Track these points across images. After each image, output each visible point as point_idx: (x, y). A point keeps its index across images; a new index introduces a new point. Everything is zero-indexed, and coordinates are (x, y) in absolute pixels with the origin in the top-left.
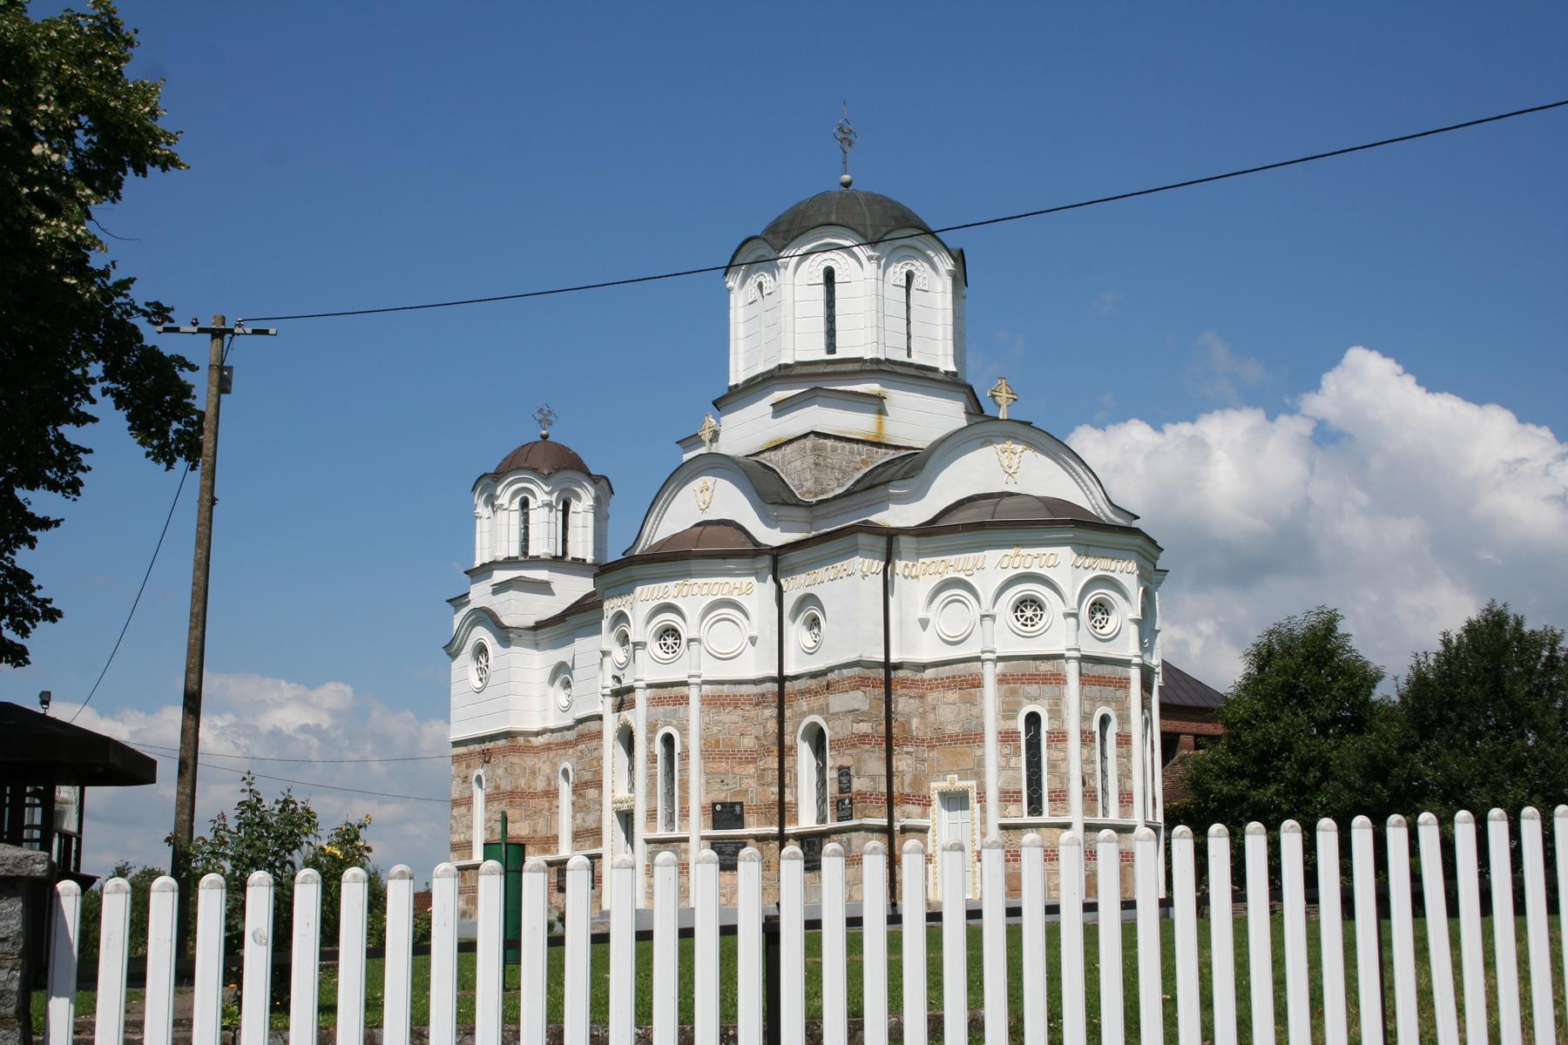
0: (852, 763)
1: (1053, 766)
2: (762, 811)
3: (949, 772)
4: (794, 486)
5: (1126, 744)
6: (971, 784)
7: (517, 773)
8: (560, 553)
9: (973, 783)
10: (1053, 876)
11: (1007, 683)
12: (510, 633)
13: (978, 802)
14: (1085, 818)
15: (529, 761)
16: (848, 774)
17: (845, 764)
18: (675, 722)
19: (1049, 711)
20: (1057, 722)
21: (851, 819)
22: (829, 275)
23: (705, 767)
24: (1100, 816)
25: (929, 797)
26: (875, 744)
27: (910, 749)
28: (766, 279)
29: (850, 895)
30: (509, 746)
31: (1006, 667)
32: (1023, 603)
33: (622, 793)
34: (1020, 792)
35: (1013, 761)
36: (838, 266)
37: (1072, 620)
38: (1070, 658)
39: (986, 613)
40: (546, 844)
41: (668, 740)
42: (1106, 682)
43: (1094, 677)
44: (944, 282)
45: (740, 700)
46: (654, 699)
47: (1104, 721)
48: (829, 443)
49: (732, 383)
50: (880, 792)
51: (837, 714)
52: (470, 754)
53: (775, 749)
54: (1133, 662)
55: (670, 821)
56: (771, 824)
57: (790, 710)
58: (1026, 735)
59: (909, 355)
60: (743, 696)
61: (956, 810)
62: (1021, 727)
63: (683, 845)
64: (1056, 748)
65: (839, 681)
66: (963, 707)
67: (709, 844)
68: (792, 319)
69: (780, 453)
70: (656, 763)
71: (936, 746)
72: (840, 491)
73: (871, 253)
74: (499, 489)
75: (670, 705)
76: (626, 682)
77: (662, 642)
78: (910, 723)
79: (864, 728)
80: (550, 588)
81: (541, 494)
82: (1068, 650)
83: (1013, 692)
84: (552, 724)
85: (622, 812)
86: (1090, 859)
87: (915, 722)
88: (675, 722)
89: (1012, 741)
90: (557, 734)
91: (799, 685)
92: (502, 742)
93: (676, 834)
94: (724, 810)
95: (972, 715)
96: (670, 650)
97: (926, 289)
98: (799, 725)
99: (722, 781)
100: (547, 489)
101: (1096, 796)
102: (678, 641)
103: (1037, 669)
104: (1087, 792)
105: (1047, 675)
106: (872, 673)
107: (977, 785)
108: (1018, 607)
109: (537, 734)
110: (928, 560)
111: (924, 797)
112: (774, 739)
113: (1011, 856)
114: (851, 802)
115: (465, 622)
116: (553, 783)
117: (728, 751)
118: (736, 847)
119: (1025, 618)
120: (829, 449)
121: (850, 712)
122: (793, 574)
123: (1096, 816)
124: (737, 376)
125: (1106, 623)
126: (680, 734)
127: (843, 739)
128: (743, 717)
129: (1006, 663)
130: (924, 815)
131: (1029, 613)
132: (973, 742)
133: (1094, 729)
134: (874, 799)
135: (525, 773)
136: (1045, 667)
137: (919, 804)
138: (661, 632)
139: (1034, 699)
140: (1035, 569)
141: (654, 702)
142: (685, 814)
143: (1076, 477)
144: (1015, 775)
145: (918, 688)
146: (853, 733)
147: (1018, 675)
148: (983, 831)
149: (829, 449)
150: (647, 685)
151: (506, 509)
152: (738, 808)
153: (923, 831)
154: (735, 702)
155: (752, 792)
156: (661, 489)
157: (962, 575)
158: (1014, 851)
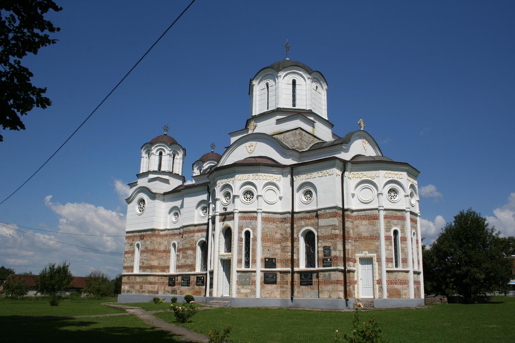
0: (331, 245)
1: (403, 250)
2: (284, 262)
3: (364, 250)
4: (290, 146)
6: (374, 255)
7: (155, 243)
8: (171, 171)
9: (375, 255)
10: (403, 290)
11: (387, 219)
12: (156, 195)
13: (377, 262)
15: (159, 240)
19: (401, 230)
21: (331, 266)
22: (294, 82)
25: (355, 259)
28: (271, 82)
30: (153, 234)
31: (386, 213)
32: (392, 190)
33: (223, 252)
34: (392, 259)
35: (390, 247)
38: (408, 211)
40: (164, 269)
41: (247, 234)
45: (275, 220)
46: (242, 217)
48: (304, 133)
49: (254, 114)
52: (134, 236)
53: (290, 239)
54: (418, 215)
55: (247, 264)
56: (288, 267)
60: (276, 218)
61: (366, 265)
62: (392, 235)
63: (253, 274)
65: (324, 214)
66: (370, 226)
67: (263, 274)
69: (282, 135)
71: (358, 240)
72: (306, 149)
73: (309, 76)
74: (153, 148)
75: (249, 220)
76: (229, 210)
77: (245, 196)
80: (169, 182)
81: (167, 151)
82: (407, 208)
83: (389, 222)
84: (168, 227)
85: (222, 260)
88: (250, 226)
89: (389, 240)
90: (170, 231)
91: (299, 215)
92: (150, 232)
93: (250, 269)
96: (248, 200)
99: (269, 250)
100: (170, 149)
102: (252, 196)
107: (376, 256)
109: (162, 230)
110: (355, 173)
112: (289, 236)
113: (390, 282)
114: (331, 260)
115: (136, 191)
116: (168, 248)
117: (271, 239)
119: (391, 196)
120: (304, 135)
121: (330, 226)
122: (298, 175)
124: (256, 113)
125: (396, 197)
128: (276, 226)
129: (386, 211)
130: (354, 266)
135: (157, 244)
136: (399, 214)
138: (245, 193)
139: (396, 225)
141: (241, 218)
142: (254, 262)
146: (332, 234)
147: (390, 216)
149: (304, 135)
150: (239, 212)
151: (154, 155)
152: (274, 260)
154: (273, 220)
155: (279, 254)
157: (370, 179)
158: (391, 281)
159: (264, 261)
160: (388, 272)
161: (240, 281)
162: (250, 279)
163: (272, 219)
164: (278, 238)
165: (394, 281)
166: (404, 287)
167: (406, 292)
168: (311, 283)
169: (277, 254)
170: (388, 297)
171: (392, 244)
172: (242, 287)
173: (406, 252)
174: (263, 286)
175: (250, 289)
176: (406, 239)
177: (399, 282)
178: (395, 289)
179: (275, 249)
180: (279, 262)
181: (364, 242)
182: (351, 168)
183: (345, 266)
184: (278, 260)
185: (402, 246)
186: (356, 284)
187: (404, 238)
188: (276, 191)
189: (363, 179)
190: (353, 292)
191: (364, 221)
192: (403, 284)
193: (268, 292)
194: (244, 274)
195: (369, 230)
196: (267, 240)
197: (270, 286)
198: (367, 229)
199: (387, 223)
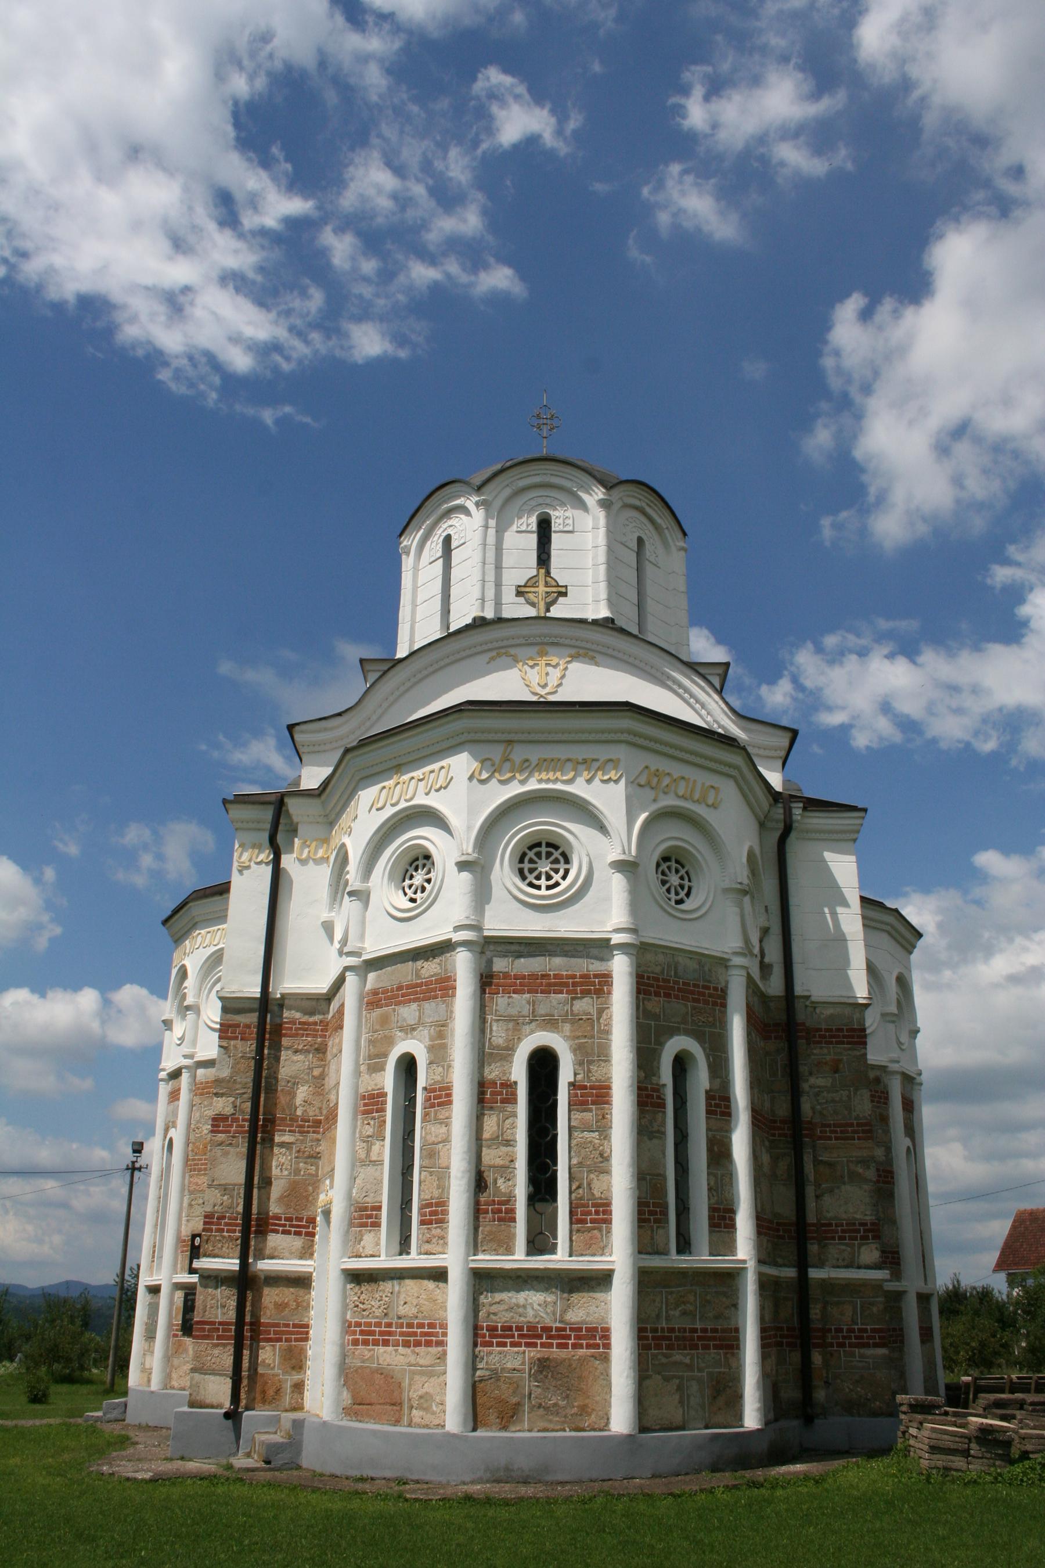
10: (417, 1378)
20: (440, 1069)
23: (190, 1182)
26: (236, 1132)
42: (549, 985)
54: (612, 943)
97: (570, 528)
101: (512, 1211)
113: (362, 1333)
119: (673, 891)
123: (510, 1251)
130: (307, 1252)
133: (513, 1078)
134: (226, 1224)
138: (404, 864)
143: (686, 695)
145: (315, 1036)
160: (570, 1256)
166: (422, 1362)
167: (431, 1390)
170: (348, 1412)
173: (444, 1165)
178: (380, 1371)
185: (428, 1137)
190: (289, 1380)
192: (418, 1344)
199: (378, 1027)
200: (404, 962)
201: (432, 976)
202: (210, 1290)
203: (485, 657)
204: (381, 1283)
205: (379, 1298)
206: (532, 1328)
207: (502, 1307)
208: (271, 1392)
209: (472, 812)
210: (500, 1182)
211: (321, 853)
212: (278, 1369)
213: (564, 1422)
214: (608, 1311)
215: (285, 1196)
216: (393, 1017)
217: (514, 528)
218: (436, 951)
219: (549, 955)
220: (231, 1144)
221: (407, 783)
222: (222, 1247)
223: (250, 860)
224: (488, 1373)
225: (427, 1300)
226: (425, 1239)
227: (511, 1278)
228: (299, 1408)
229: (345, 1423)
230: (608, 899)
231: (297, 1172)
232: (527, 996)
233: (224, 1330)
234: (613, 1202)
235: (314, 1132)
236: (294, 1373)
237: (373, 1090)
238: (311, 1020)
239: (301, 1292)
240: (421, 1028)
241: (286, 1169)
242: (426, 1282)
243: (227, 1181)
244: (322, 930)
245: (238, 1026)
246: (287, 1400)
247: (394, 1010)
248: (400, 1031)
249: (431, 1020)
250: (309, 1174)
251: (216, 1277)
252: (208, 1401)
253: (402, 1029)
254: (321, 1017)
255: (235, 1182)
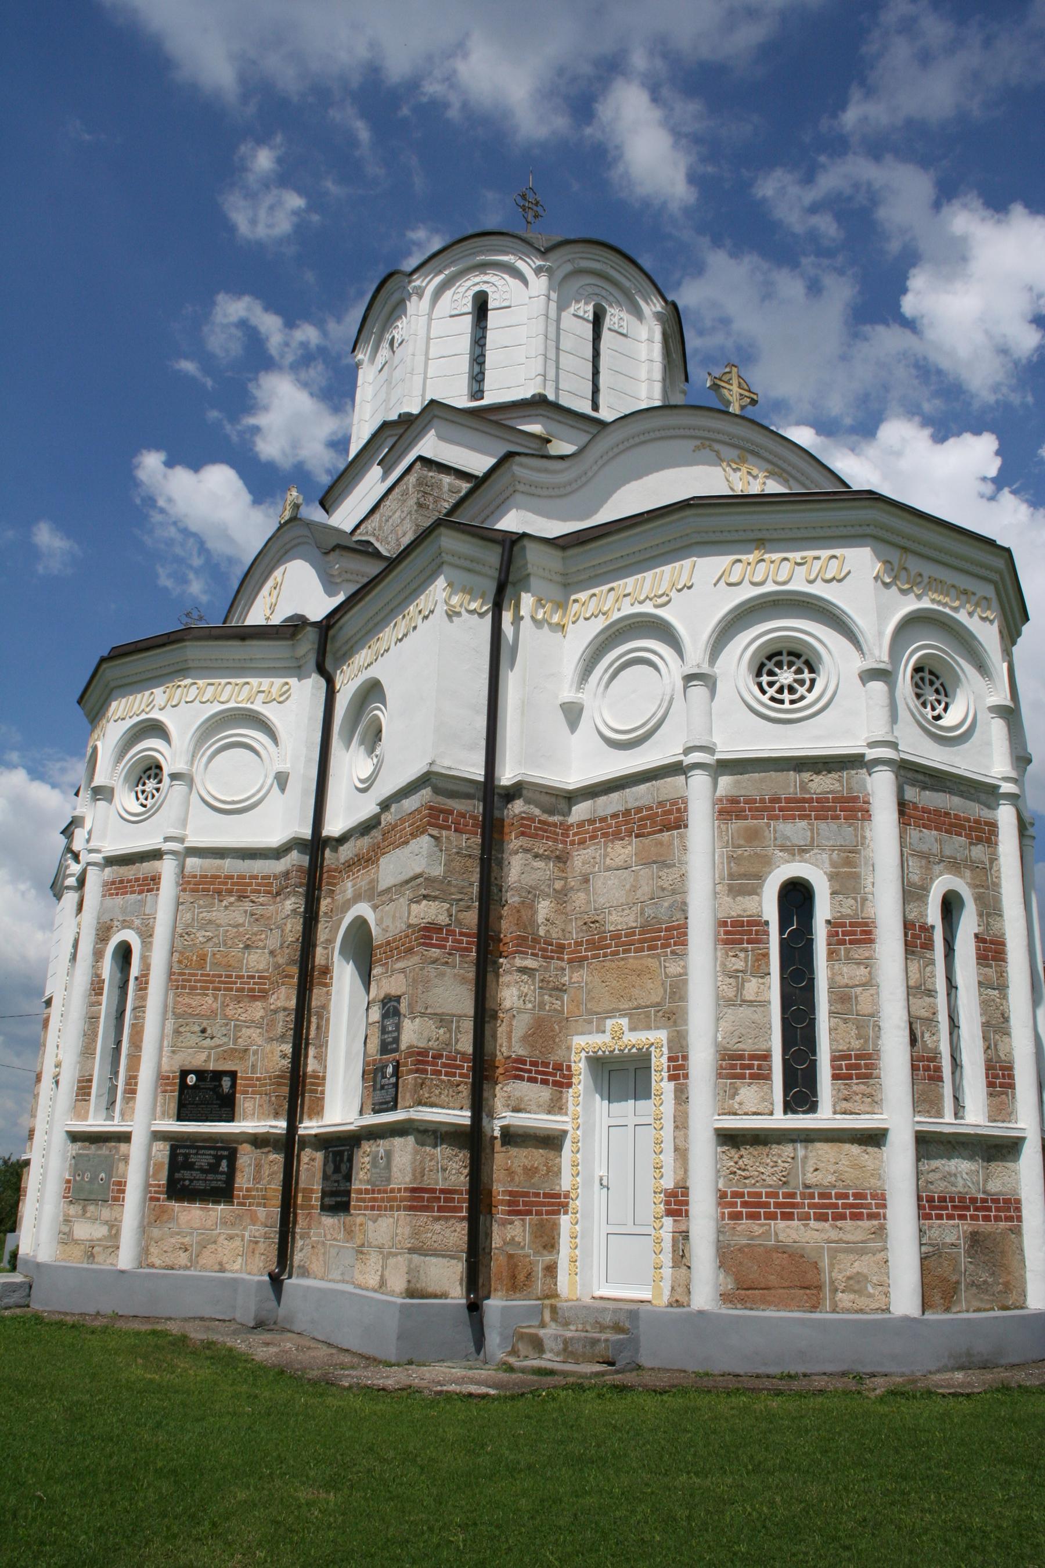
0: (403, 989)
1: (842, 997)
3: (611, 1013)
5: (994, 959)
9: (660, 1036)
10: (841, 1256)
11: (738, 818)
13: (671, 1078)
14: (917, 1119)
16: (397, 1013)
17: (394, 992)
18: (137, 922)
19: (832, 877)
20: (852, 902)
21: (395, 1108)
23: (176, 1003)
24: (949, 1117)
25: (569, 1068)
26: (453, 948)
27: (530, 963)
29: (382, 1276)
31: (738, 782)
34: (767, 1057)
35: (751, 987)
36: (494, 289)
37: (878, 687)
38: (878, 762)
39: (696, 671)
41: (124, 953)
42: (951, 825)
43: (924, 810)
44: (650, 329)
45: (250, 885)
46: (113, 883)
47: (951, 905)
50: (458, 1052)
51: (388, 890)
54: (1002, 791)
57: (329, 900)
58: (782, 931)
59: (595, 407)
60: (255, 877)
62: (770, 912)
64: (848, 958)
66: (644, 872)
67: (168, 1148)
68: (423, 358)
70: (101, 994)
71: (586, 958)
73: (539, 263)
78: (532, 908)
79: (431, 912)
82: (872, 745)
83: (753, 836)
86: (928, 1217)
87: (544, 908)
94: (202, 1084)
95: (663, 889)
97: (625, 332)
98: (341, 923)
99: (204, 1031)
101: (938, 1069)
103: (804, 787)
104: (922, 1059)
105: (827, 800)
106: (458, 805)
107: (669, 1041)
108: (762, 665)
111: (558, 1067)
113: (745, 1204)
114: (396, 1073)
117: (221, 976)
118: (215, 1157)
123: (940, 1114)
126: (143, 942)
127: (394, 941)
130: (556, 1106)
131: (786, 677)
132: (664, 946)
133: (765, 918)
134: (445, 1065)
136: (822, 784)
137: (545, 1082)
139: (798, 851)
140: (799, 585)
144: (756, 1017)
145: (556, 841)
147: (762, 801)
148: (681, 1145)
152: (226, 1083)
153: (552, 1141)
155: (256, 1053)
156: (229, 611)
159: (177, 1088)
161: (75, 1179)
162: (110, 1176)
163: (233, 884)
164: (258, 971)
165: (775, 1195)
168: (344, 1199)
169: (246, 1050)
170: (726, 1298)
171: (768, 964)
172: (80, 1212)
174: (163, 1211)
175: (106, 1223)
176: (869, 933)
177: (811, 1206)
178: (781, 1249)
179: (235, 1026)
180: (253, 1093)
181: (613, 965)
182: (564, 575)
183: (479, 1106)
184: (247, 1079)
185: (838, 978)
186: (566, 1213)
187: (851, 925)
188: (265, 748)
189: (616, 616)
191: (618, 844)
193: (186, 1240)
194: (93, 1147)
195: (639, 892)
196: (199, 981)
197: (198, 1212)
198: (628, 887)
200: (782, 770)
201: (828, 793)
202: (428, 1149)
203: (692, 443)
204: (774, 1146)
205: (772, 1164)
206: (962, 1199)
207: (937, 1176)
208: (521, 1277)
209: (882, 618)
210: (927, 1035)
211: (555, 619)
212: (529, 1248)
213: (993, 1301)
214: (1018, 1182)
215: (529, 1036)
216: (767, 833)
217: (572, 310)
218: (831, 765)
219: (949, 793)
220: (447, 963)
221: (753, 565)
222: (440, 1093)
223: (461, 606)
224: (931, 1249)
225: (853, 1166)
226: (841, 1095)
227: (942, 1143)
228: (555, 1295)
229: (724, 1311)
230: (989, 744)
231: (542, 1005)
232: (934, 832)
233: (446, 1200)
234: (1016, 1066)
235: (559, 959)
236: (545, 1252)
237: (739, 916)
238: (551, 819)
239: (551, 1154)
240: (816, 851)
241: (530, 1002)
242: (847, 1146)
243: (444, 1011)
244: (560, 712)
245: (451, 812)
246: (539, 1285)
247: (768, 825)
248: (781, 851)
249: (831, 843)
250: (555, 1010)
251: (435, 1132)
252: (430, 1290)
253: (783, 848)
254: (561, 818)
255: (454, 1012)
